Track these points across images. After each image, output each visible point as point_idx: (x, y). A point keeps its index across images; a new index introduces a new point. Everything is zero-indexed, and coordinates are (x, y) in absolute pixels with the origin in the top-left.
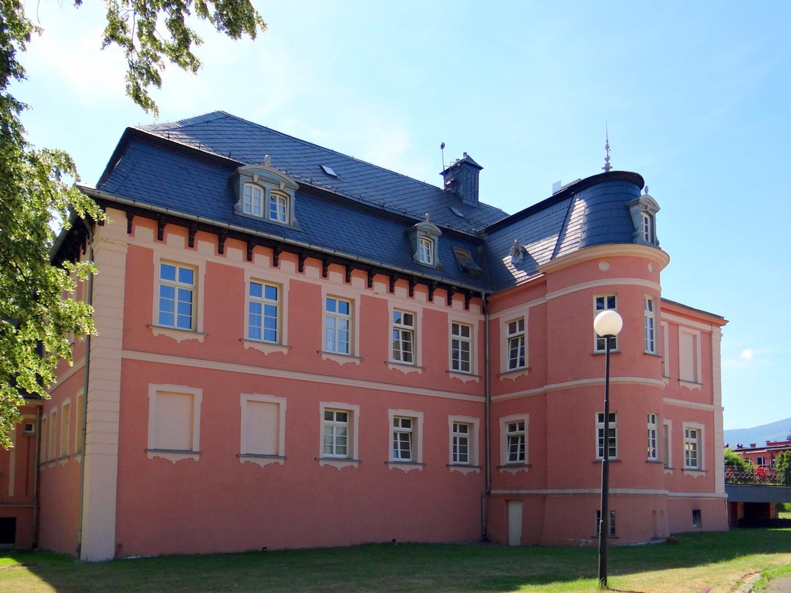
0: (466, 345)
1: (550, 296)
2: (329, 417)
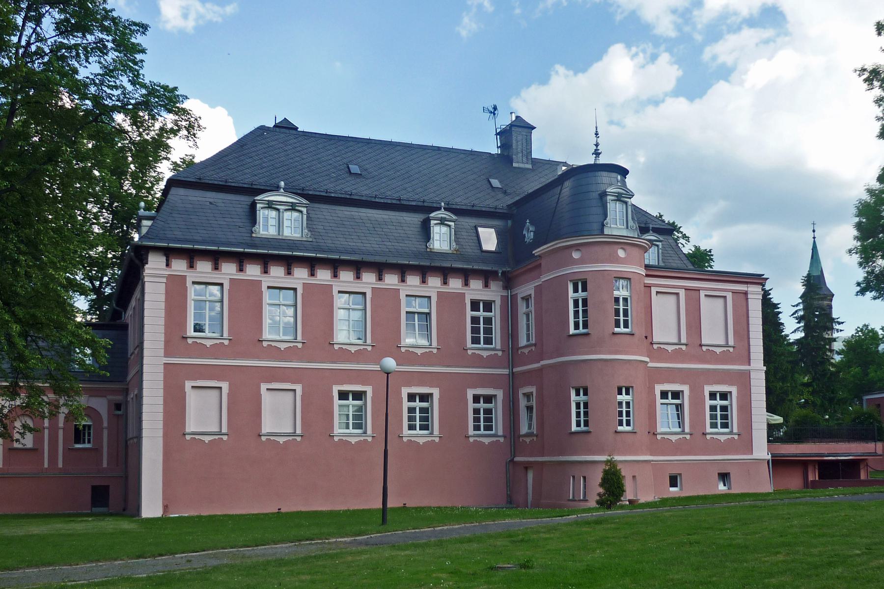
0: (488, 321)
1: (545, 278)
2: (343, 395)
